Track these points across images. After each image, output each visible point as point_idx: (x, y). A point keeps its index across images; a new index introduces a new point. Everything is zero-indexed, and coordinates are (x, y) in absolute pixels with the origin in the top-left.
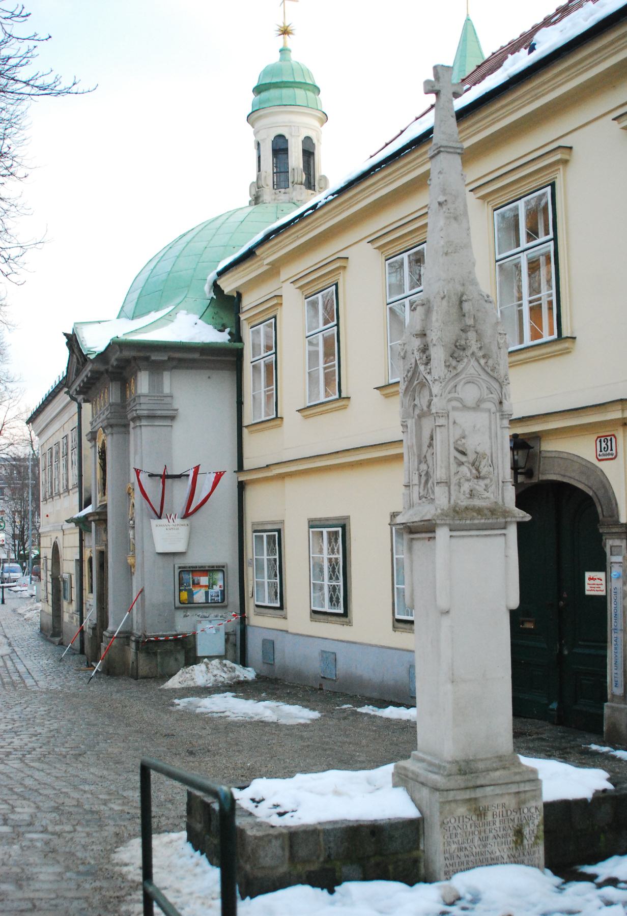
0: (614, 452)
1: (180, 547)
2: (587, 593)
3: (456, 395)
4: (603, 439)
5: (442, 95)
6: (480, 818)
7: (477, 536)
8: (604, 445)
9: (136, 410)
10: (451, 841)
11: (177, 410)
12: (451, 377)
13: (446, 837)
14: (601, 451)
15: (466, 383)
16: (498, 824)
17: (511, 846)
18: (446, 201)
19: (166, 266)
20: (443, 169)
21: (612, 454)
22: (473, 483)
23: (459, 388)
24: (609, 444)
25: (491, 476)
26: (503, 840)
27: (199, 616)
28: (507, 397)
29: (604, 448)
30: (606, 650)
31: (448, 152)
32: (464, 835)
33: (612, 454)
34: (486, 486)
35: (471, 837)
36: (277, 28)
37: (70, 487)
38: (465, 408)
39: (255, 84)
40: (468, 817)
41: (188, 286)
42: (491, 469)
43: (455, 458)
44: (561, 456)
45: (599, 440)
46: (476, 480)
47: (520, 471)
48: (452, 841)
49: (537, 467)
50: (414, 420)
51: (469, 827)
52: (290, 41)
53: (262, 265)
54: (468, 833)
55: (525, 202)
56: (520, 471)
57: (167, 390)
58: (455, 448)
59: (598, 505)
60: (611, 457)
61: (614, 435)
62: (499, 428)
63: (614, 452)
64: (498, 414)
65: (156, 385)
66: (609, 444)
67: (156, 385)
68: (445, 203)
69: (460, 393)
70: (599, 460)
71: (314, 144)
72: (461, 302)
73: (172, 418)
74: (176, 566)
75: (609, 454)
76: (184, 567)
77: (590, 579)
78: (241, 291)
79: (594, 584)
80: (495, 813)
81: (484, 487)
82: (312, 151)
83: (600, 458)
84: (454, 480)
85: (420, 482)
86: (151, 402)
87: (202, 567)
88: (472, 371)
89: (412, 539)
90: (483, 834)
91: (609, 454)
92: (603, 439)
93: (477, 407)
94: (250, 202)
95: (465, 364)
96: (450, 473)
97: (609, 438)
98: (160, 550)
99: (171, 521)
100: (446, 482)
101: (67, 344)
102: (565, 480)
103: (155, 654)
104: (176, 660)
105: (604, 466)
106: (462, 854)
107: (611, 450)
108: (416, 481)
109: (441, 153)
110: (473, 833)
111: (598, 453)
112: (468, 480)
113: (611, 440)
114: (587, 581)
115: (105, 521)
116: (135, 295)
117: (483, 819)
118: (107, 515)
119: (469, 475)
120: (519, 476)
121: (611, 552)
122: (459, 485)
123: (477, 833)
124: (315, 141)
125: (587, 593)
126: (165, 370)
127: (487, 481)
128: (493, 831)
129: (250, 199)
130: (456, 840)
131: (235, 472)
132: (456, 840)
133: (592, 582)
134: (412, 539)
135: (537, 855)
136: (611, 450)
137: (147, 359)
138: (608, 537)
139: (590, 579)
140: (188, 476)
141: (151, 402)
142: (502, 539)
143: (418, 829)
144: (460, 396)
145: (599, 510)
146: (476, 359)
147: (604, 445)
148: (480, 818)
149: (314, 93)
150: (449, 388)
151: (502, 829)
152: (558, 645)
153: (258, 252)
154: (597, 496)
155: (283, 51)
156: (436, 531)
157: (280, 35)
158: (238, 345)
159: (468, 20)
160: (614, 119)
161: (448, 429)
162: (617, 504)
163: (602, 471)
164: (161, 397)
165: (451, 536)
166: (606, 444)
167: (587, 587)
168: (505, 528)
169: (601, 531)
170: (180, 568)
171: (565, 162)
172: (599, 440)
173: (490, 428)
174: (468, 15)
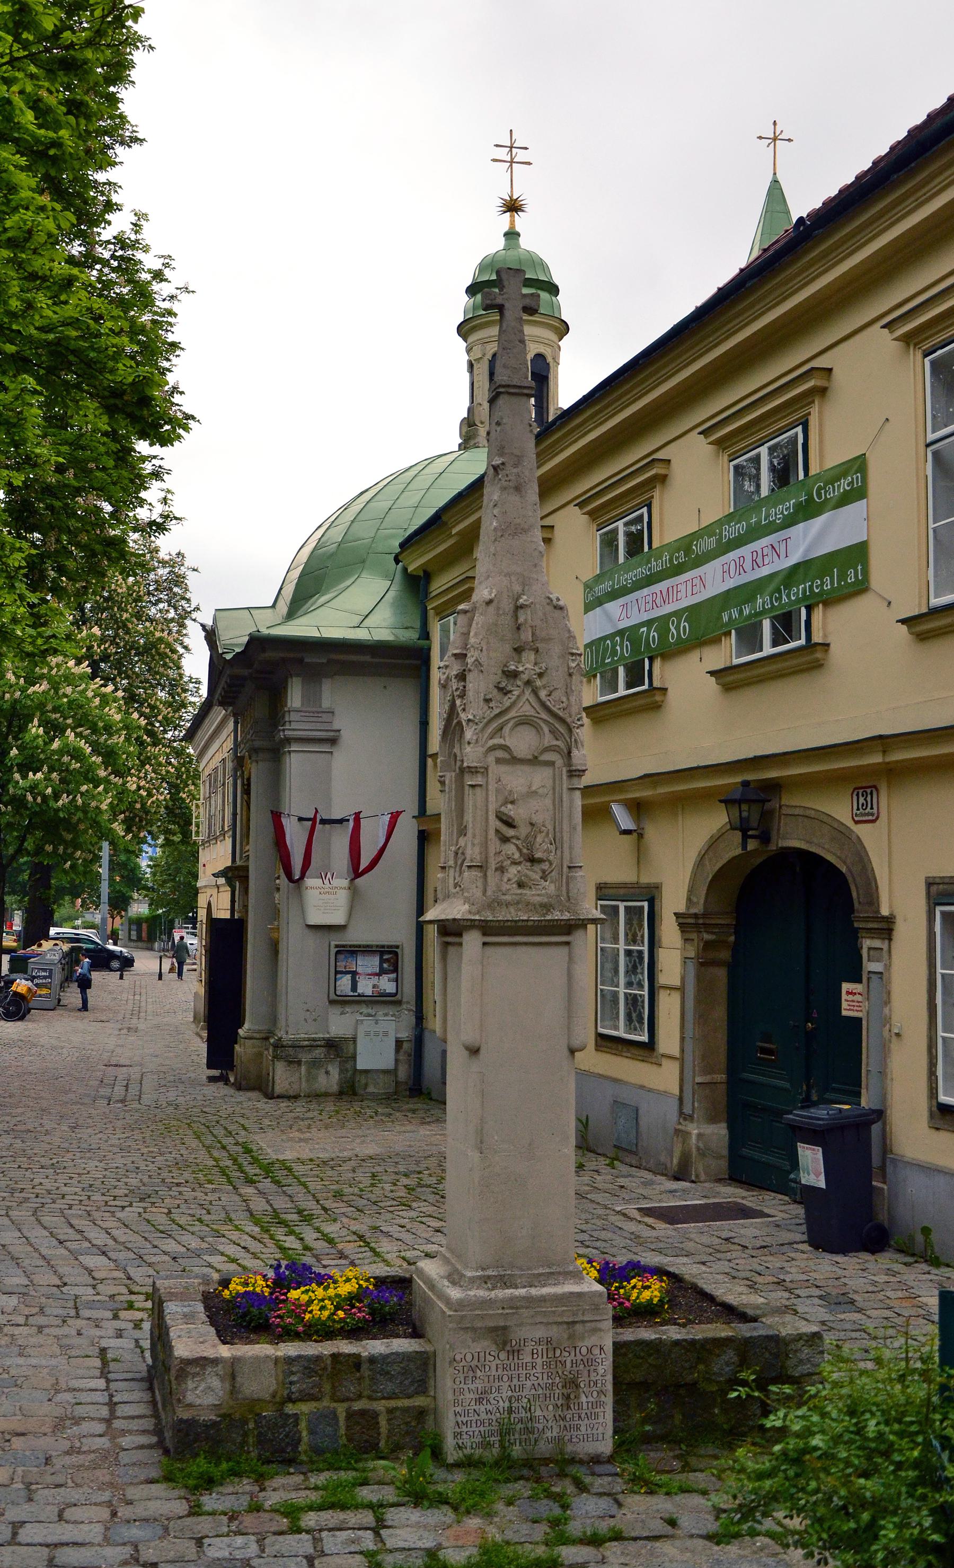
0: (875, 811)
1: (338, 918)
2: (844, 1013)
3: (501, 741)
4: (861, 791)
5: (507, 313)
6: (511, 1357)
7: (526, 944)
8: (862, 800)
9: (284, 730)
10: (465, 1387)
11: (339, 731)
12: (492, 715)
13: (457, 1380)
14: (858, 809)
15: (517, 725)
16: (538, 1367)
17: (559, 1403)
18: (503, 464)
19: (337, 534)
20: (502, 418)
21: (872, 814)
22: (524, 868)
23: (507, 729)
24: (869, 799)
25: (551, 858)
26: (548, 1392)
27: (361, 1013)
28: (580, 746)
29: (863, 805)
30: (860, 1098)
31: (509, 393)
32: (486, 1380)
33: (872, 814)
34: (544, 871)
35: (497, 1384)
36: (500, 202)
37: (226, 829)
38: (515, 760)
39: (469, 282)
40: (492, 1353)
41: (364, 562)
42: (553, 848)
43: (497, 831)
44: (808, 813)
45: (855, 793)
46: (529, 864)
47: (750, 833)
48: (466, 1389)
49: (776, 827)
50: (453, 774)
51: (494, 1368)
52: (522, 222)
53: (450, 536)
54: (491, 1378)
55: (769, 448)
56: (750, 833)
57: (326, 704)
58: (497, 816)
59: (853, 888)
60: (870, 818)
61: (875, 787)
62: (565, 790)
63: (875, 811)
64: (564, 770)
65: (312, 698)
66: (869, 799)
67: (312, 698)
68: (501, 467)
69: (507, 739)
70: (857, 822)
71: (548, 364)
72: (518, 608)
73: (333, 741)
74: (333, 943)
75: (868, 814)
76: (343, 946)
77: (848, 993)
78: (429, 569)
79: (853, 1001)
80: (535, 1351)
81: (540, 874)
82: (544, 374)
83: (856, 819)
84: (493, 865)
85: (456, 863)
86: (304, 719)
87: (368, 946)
88: (527, 707)
89: (447, 944)
90: (515, 1381)
91: (868, 814)
92: (861, 791)
93: (534, 761)
94: (460, 445)
95: (514, 698)
96: (487, 854)
97: (869, 791)
98: (314, 919)
99: (326, 882)
100: (481, 867)
101: (206, 638)
102: (813, 849)
103: (299, 1063)
104: (327, 1073)
105: (863, 831)
106: (482, 1408)
107: (872, 808)
108: (451, 863)
109: (501, 396)
110: (500, 1379)
111: (855, 811)
112: (515, 863)
113: (871, 794)
114: (844, 996)
115: (247, 877)
116: (296, 574)
117: (516, 1358)
118: (248, 871)
119: (517, 856)
120: (749, 840)
121: (869, 956)
122: (501, 869)
123: (505, 1378)
124: (549, 360)
125: (844, 1013)
126: (326, 676)
127: (545, 866)
128: (532, 1378)
129: (461, 441)
130: (472, 1387)
131: (414, 817)
132: (472, 1387)
133: (850, 997)
134: (447, 944)
135: (601, 1420)
136: (872, 808)
137: (301, 661)
138: (864, 935)
139: (848, 993)
140: (348, 820)
141: (304, 719)
142: (564, 950)
143: (425, 1364)
144: (508, 744)
145: (854, 894)
146: (533, 690)
147: (862, 800)
148: (511, 1357)
149: (550, 293)
150: (490, 730)
151: (545, 1376)
152: (805, 1087)
153: (444, 518)
154: (852, 874)
155: (512, 235)
156: (464, 935)
157: (505, 212)
158: (423, 643)
159: (775, 182)
160: (883, 327)
161: (487, 790)
162: (877, 888)
163: (858, 837)
164: (318, 713)
165: (484, 944)
166: (865, 799)
167: (844, 1005)
168: (569, 933)
169: (856, 925)
170: (337, 946)
171: (822, 391)
172: (855, 793)
173: (554, 789)
174: (775, 174)
